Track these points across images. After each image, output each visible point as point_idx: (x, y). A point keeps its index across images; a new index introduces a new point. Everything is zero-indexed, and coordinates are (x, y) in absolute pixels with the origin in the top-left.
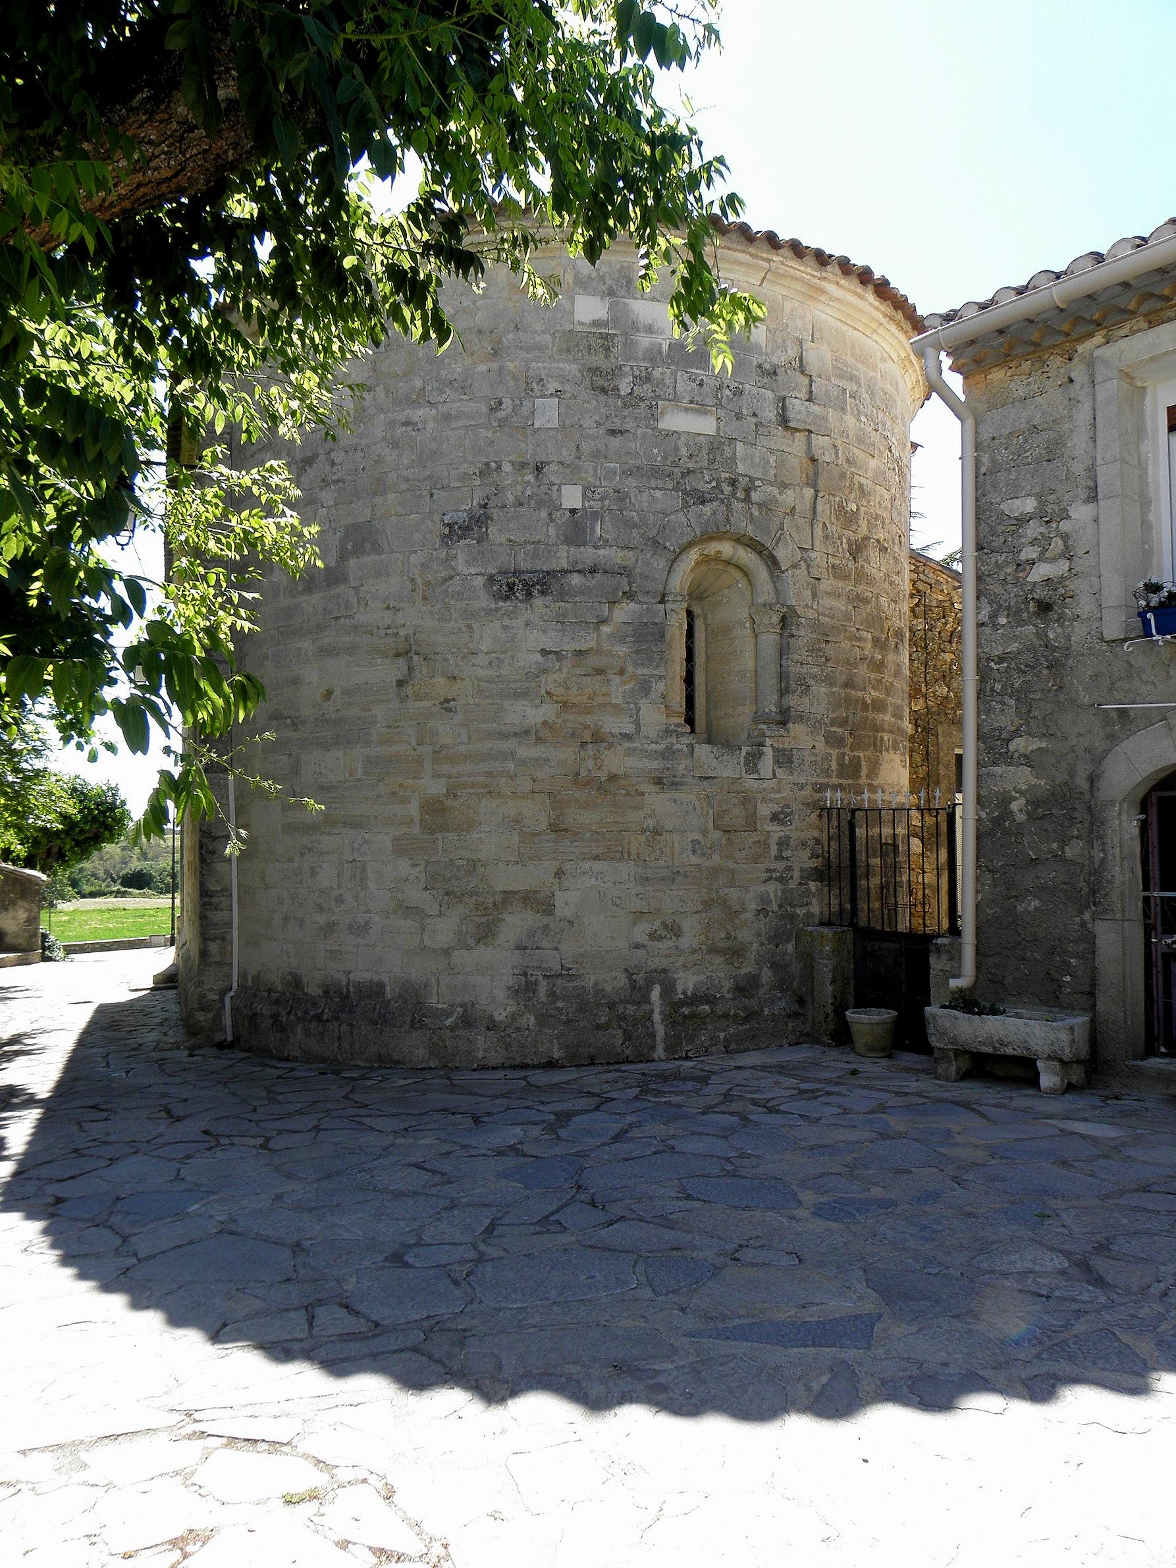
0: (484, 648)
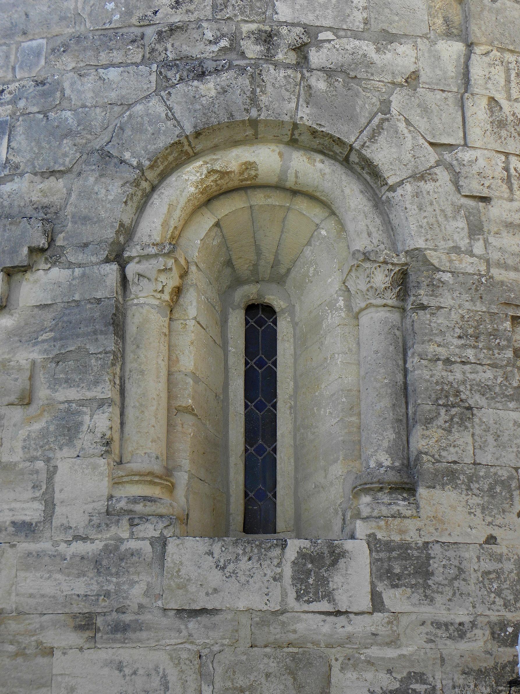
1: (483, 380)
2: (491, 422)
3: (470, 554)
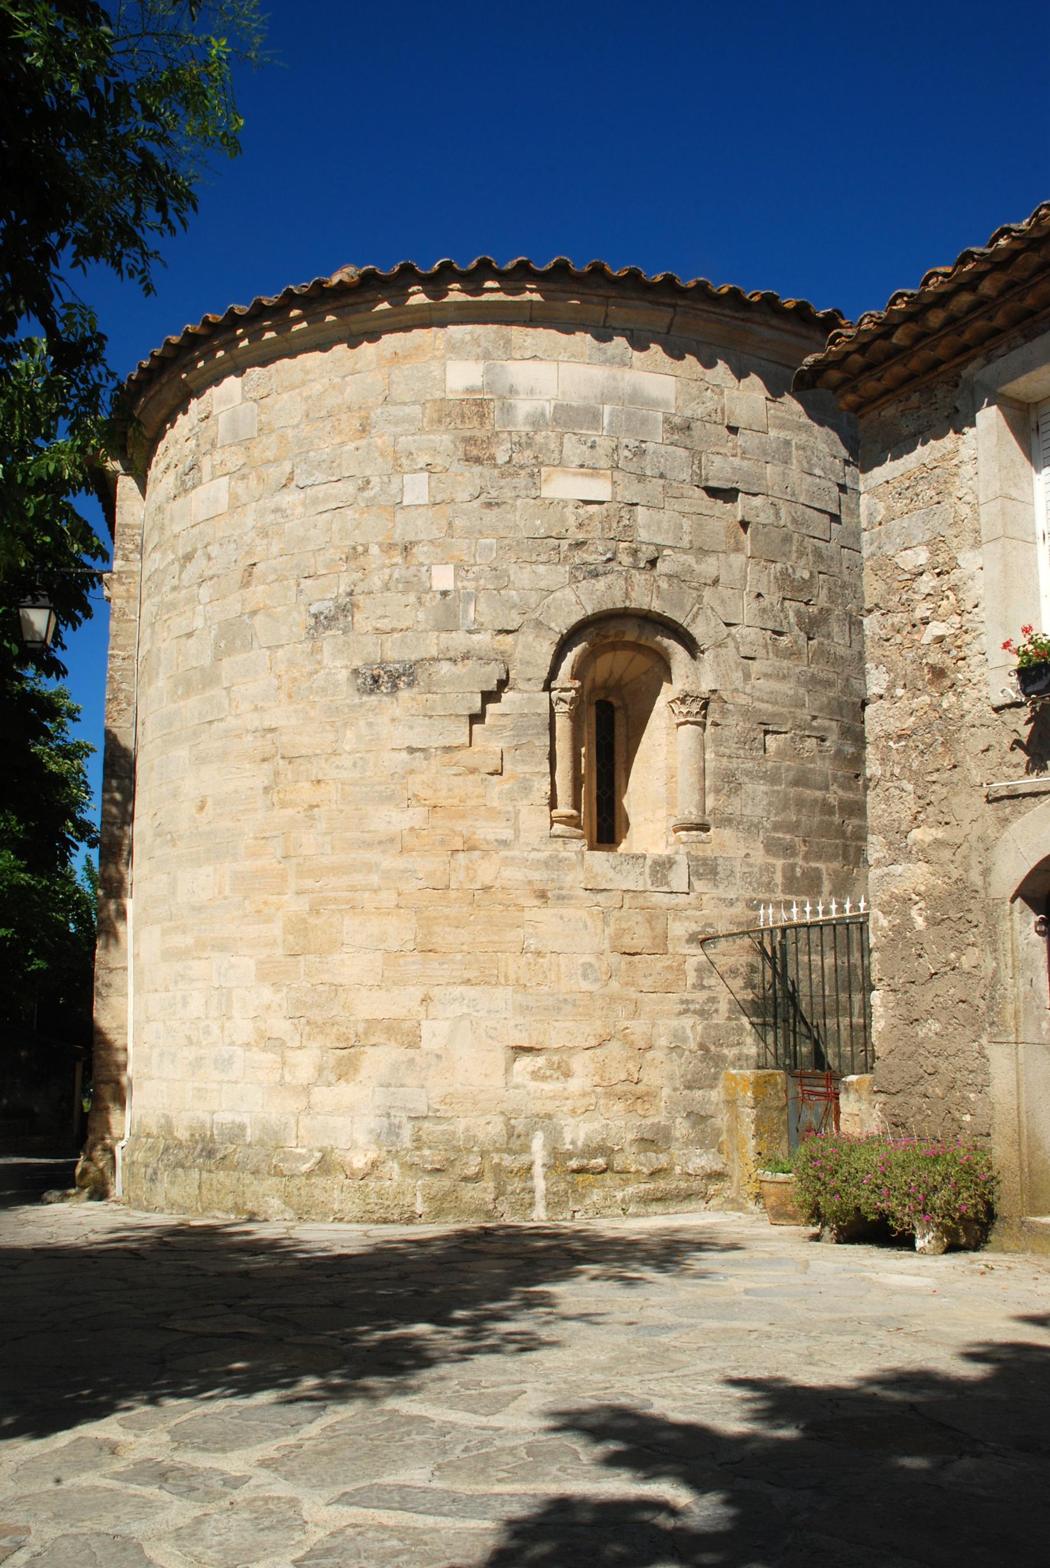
0: (347, 748)
3: (738, 863)
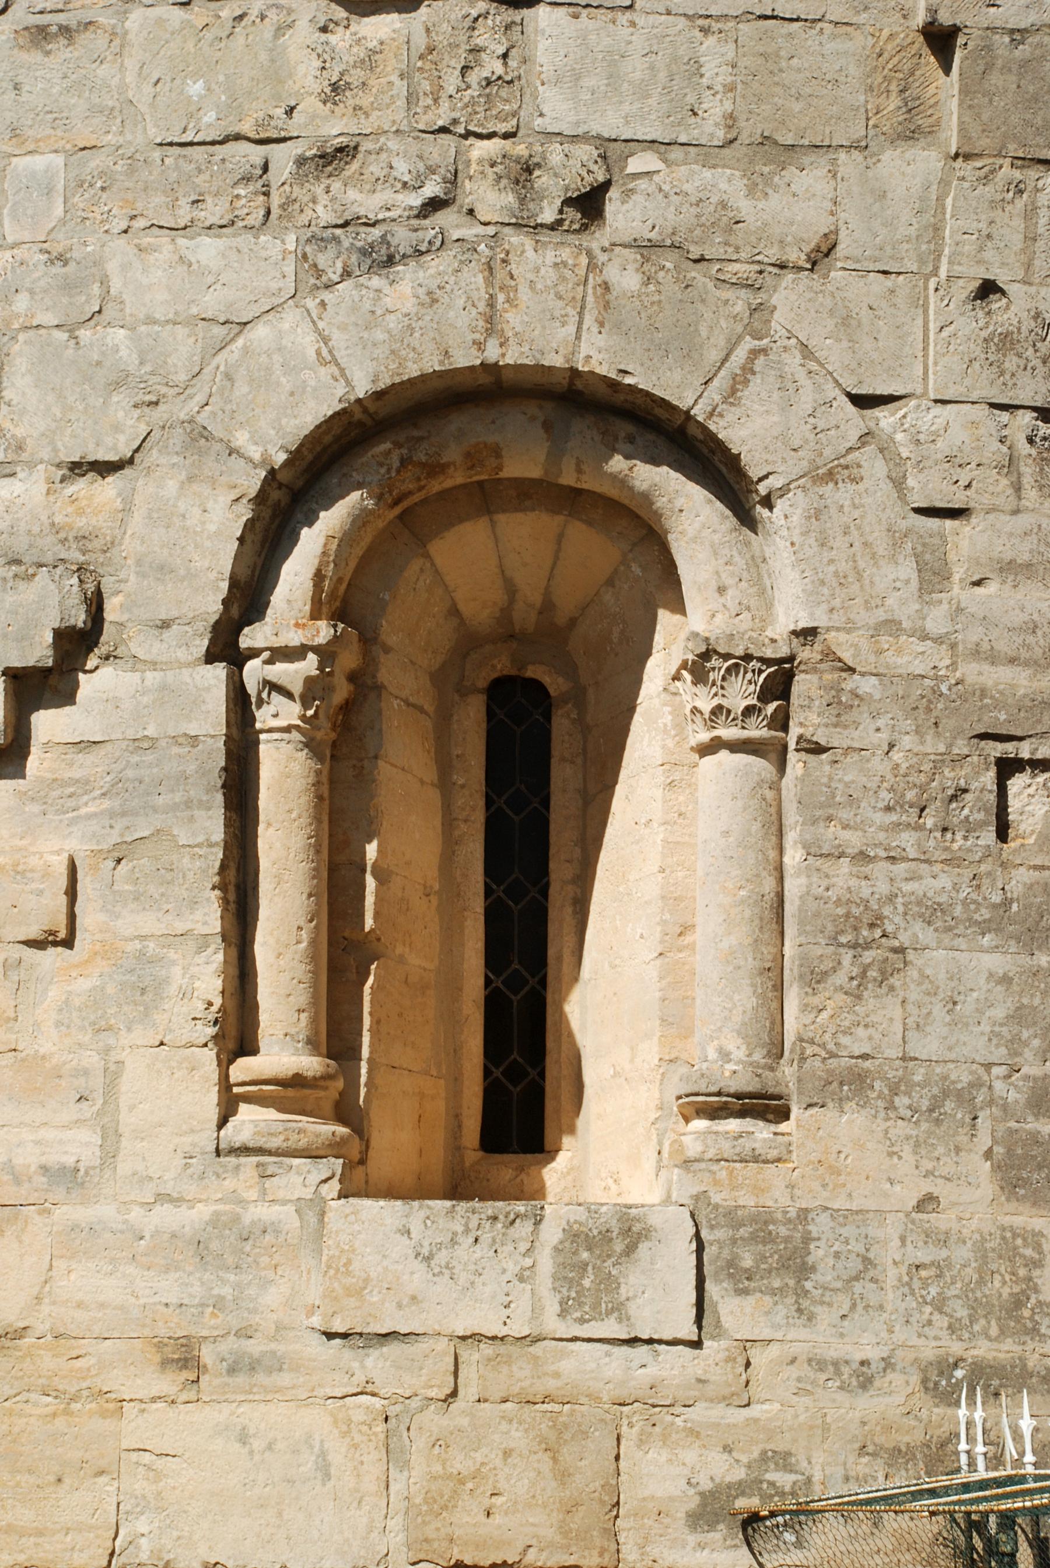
1: (930, 894)
2: (942, 976)
